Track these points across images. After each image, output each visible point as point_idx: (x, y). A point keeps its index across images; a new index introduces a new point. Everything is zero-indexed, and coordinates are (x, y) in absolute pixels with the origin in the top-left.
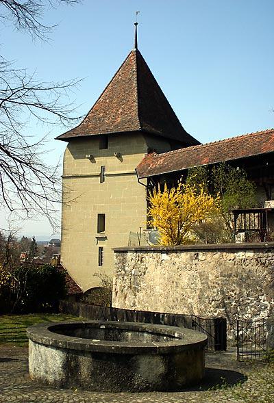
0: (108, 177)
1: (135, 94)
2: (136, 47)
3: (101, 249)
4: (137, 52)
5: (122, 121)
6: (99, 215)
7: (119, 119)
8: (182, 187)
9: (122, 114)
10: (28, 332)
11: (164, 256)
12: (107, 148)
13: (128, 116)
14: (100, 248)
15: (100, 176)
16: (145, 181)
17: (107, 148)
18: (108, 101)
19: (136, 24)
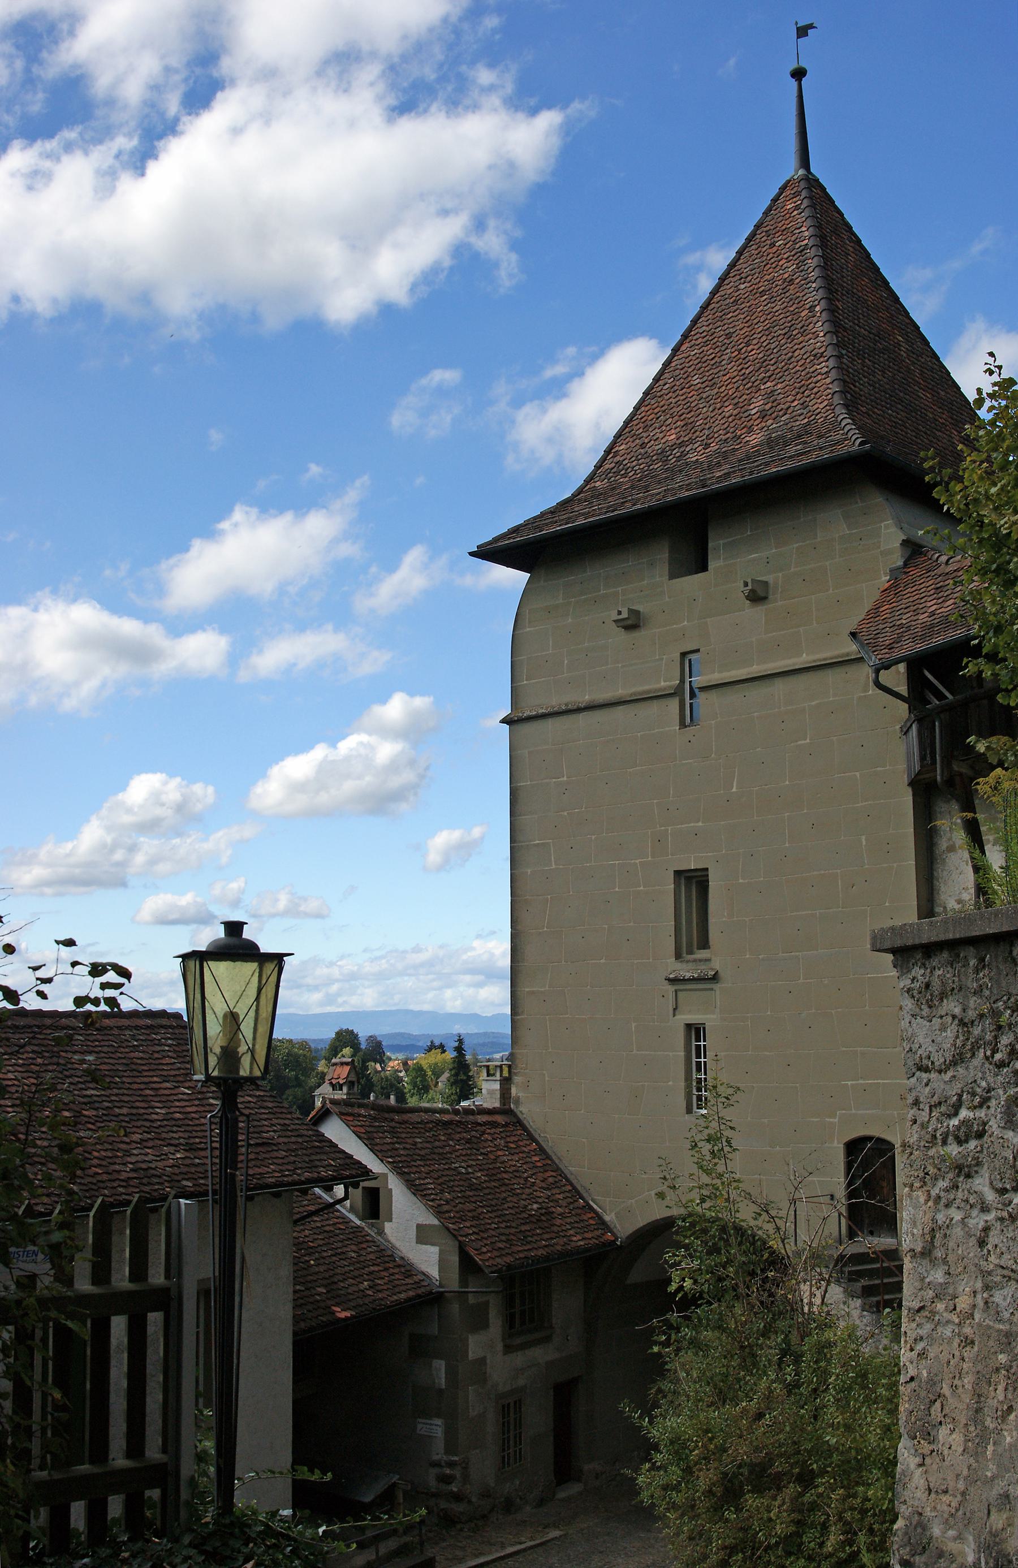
0: (713, 696)
1: (820, 327)
2: (804, 159)
3: (695, 1031)
4: (813, 184)
5: (770, 443)
6: (678, 873)
7: (755, 439)
8: (683, 1365)
9: (763, 415)
10: (430, 1552)
11: (312, 1208)
12: (703, 568)
13: (962, 1536)
14: (689, 1026)
15: (677, 692)
16: (897, 678)
17: (703, 568)
18: (696, 380)
19: (799, 74)
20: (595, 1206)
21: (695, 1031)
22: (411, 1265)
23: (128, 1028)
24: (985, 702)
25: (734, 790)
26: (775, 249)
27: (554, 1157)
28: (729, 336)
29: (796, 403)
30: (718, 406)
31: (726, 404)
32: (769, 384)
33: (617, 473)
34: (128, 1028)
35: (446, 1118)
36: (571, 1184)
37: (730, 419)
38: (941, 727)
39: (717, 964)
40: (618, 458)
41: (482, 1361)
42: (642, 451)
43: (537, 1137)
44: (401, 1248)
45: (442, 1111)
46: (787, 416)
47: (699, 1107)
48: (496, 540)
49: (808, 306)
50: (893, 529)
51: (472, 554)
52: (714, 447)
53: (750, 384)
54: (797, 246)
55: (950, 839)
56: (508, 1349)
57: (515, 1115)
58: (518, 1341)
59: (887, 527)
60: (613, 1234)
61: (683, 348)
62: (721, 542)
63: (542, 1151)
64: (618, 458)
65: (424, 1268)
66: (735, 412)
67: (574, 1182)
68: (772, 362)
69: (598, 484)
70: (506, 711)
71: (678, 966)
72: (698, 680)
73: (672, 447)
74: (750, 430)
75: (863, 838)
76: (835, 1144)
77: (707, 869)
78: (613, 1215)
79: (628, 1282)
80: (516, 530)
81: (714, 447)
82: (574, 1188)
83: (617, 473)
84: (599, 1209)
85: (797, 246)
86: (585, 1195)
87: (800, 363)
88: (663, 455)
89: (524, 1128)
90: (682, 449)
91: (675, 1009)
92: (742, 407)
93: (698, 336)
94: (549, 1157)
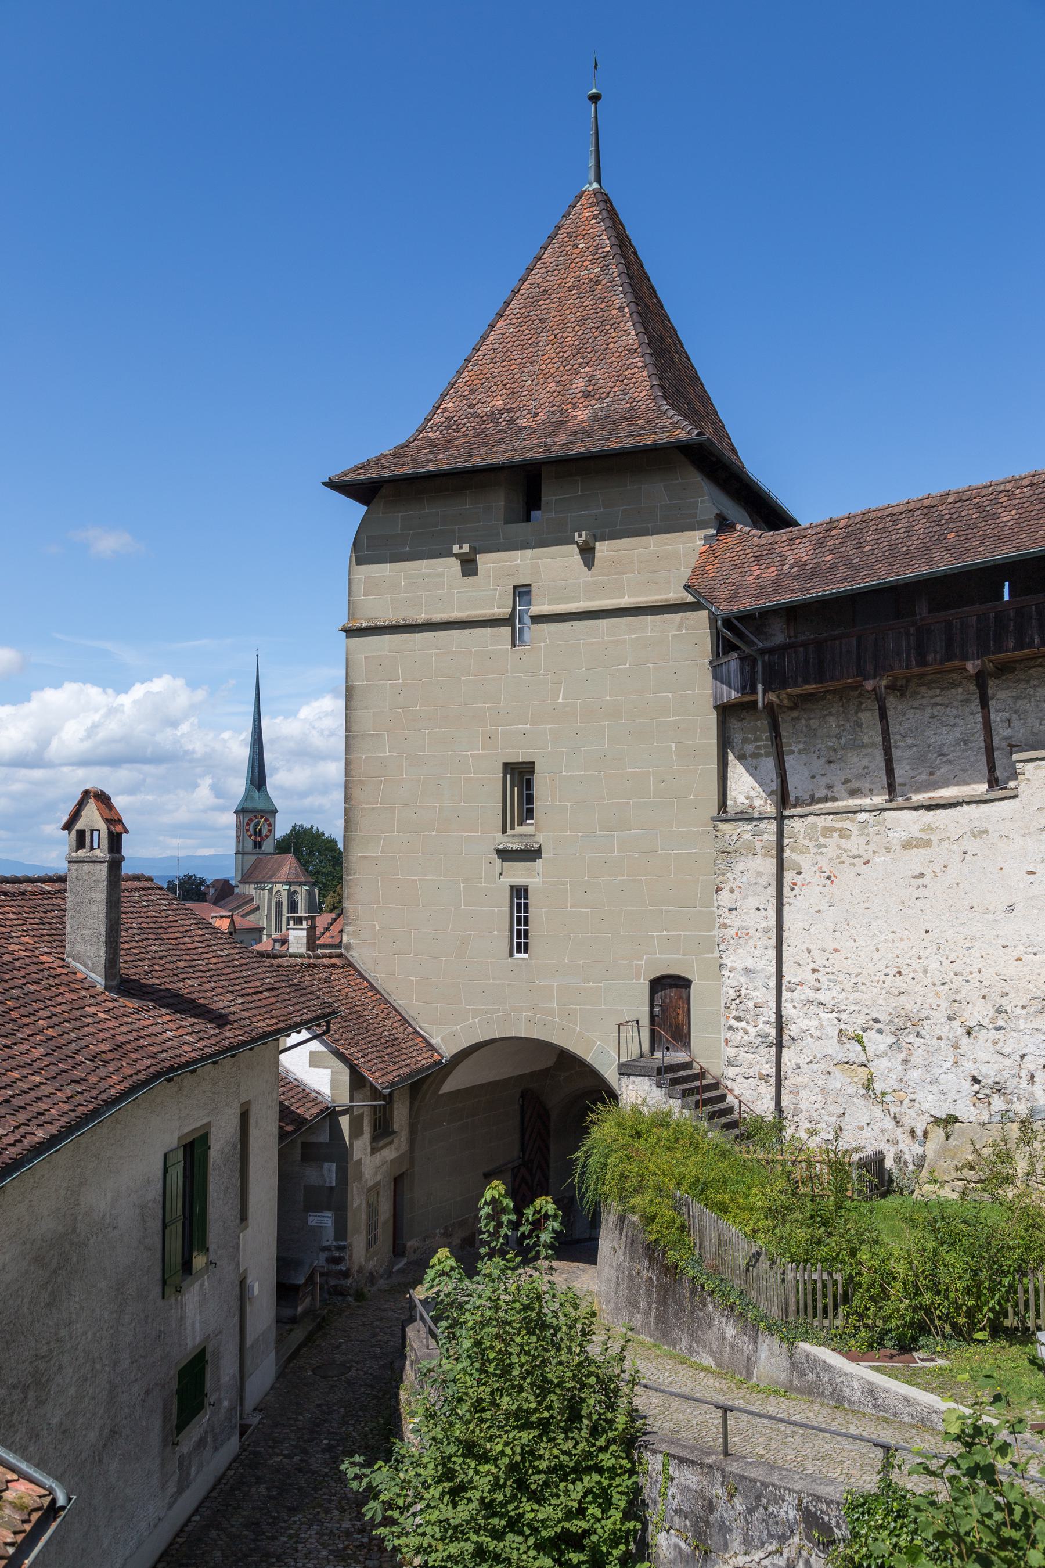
3: (519, 892)
6: (505, 765)
20: (422, 1032)
21: (519, 892)
22: (305, 1085)
23: (136, 889)
24: (801, 649)
25: (560, 700)
26: (577, 251)
27: (383, 992)
28: (542, 321)
29: (616, 389)
30: (541, 381)
31: (549, 380)
32: (587, 369)
33: (448, 428)
34: (136, 889)
35: (306, 961)
36: (400, 1015)
37: (555, 394)
38: (763, 667)
39: (540, 839)
40: (447, 414)
41: (360, 1161)
42: (471, 411)
43: (367, 976)
44: (295, 1071)
45: (301, 956)
46: (609, 399)
47: (519, 951)
48: (344, 474)
49: (617, 306)
50: (709, 504)
51: (324, 484)
52: (542, 417)
53: (569, 367)
54: (600, 251)
55: (742, 749)
56: (374, 1151)
57: (346, 958)
58: (381, 1143)
59: (703, 502)
60: (439, 1054)
61: (499, 325)
62: (554, 498)
63: (372, 987)
64: (447, 414)
65: (317, 1087)
66: (558, 389)
67: (403, 1013)
68: (589, 350)
69: (430, 434)
70: (343, 621)
71: (504, 839)
72: (535, 610)
73: (501, 412)
74: (575, 407)
75: (673, 745)
76: (642, 980)
77: (533, 763)
78: (439, 1039)
79: (441, 1092)
80: (365, 466)
81: (542, 417)
82: (403, 1018)
83: (448, 428)
84: (425, 1034)
85: (600, 251)
86: (413, 1023)
87: (616, 355)
88: (492, 417)
89: (356, 969)
90: (511, 414)
91: (501, 874)
92: (564, 386)
93: (512, 316)
94: (378, 992)
